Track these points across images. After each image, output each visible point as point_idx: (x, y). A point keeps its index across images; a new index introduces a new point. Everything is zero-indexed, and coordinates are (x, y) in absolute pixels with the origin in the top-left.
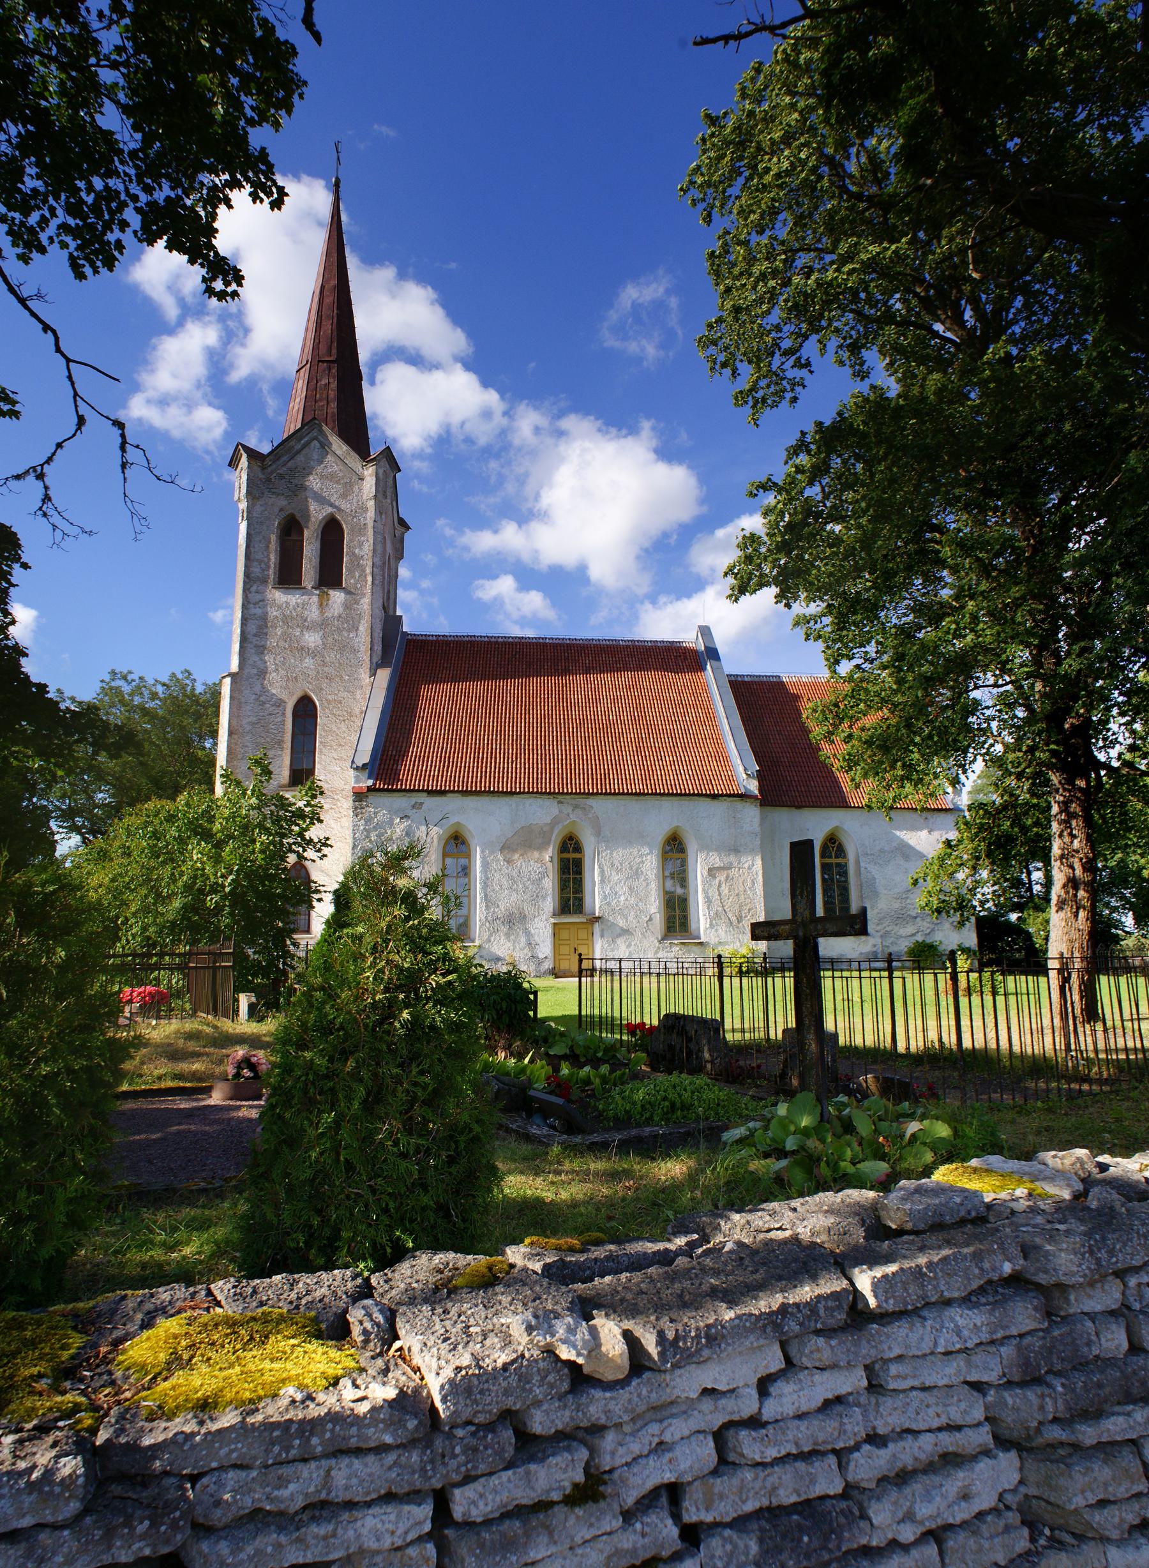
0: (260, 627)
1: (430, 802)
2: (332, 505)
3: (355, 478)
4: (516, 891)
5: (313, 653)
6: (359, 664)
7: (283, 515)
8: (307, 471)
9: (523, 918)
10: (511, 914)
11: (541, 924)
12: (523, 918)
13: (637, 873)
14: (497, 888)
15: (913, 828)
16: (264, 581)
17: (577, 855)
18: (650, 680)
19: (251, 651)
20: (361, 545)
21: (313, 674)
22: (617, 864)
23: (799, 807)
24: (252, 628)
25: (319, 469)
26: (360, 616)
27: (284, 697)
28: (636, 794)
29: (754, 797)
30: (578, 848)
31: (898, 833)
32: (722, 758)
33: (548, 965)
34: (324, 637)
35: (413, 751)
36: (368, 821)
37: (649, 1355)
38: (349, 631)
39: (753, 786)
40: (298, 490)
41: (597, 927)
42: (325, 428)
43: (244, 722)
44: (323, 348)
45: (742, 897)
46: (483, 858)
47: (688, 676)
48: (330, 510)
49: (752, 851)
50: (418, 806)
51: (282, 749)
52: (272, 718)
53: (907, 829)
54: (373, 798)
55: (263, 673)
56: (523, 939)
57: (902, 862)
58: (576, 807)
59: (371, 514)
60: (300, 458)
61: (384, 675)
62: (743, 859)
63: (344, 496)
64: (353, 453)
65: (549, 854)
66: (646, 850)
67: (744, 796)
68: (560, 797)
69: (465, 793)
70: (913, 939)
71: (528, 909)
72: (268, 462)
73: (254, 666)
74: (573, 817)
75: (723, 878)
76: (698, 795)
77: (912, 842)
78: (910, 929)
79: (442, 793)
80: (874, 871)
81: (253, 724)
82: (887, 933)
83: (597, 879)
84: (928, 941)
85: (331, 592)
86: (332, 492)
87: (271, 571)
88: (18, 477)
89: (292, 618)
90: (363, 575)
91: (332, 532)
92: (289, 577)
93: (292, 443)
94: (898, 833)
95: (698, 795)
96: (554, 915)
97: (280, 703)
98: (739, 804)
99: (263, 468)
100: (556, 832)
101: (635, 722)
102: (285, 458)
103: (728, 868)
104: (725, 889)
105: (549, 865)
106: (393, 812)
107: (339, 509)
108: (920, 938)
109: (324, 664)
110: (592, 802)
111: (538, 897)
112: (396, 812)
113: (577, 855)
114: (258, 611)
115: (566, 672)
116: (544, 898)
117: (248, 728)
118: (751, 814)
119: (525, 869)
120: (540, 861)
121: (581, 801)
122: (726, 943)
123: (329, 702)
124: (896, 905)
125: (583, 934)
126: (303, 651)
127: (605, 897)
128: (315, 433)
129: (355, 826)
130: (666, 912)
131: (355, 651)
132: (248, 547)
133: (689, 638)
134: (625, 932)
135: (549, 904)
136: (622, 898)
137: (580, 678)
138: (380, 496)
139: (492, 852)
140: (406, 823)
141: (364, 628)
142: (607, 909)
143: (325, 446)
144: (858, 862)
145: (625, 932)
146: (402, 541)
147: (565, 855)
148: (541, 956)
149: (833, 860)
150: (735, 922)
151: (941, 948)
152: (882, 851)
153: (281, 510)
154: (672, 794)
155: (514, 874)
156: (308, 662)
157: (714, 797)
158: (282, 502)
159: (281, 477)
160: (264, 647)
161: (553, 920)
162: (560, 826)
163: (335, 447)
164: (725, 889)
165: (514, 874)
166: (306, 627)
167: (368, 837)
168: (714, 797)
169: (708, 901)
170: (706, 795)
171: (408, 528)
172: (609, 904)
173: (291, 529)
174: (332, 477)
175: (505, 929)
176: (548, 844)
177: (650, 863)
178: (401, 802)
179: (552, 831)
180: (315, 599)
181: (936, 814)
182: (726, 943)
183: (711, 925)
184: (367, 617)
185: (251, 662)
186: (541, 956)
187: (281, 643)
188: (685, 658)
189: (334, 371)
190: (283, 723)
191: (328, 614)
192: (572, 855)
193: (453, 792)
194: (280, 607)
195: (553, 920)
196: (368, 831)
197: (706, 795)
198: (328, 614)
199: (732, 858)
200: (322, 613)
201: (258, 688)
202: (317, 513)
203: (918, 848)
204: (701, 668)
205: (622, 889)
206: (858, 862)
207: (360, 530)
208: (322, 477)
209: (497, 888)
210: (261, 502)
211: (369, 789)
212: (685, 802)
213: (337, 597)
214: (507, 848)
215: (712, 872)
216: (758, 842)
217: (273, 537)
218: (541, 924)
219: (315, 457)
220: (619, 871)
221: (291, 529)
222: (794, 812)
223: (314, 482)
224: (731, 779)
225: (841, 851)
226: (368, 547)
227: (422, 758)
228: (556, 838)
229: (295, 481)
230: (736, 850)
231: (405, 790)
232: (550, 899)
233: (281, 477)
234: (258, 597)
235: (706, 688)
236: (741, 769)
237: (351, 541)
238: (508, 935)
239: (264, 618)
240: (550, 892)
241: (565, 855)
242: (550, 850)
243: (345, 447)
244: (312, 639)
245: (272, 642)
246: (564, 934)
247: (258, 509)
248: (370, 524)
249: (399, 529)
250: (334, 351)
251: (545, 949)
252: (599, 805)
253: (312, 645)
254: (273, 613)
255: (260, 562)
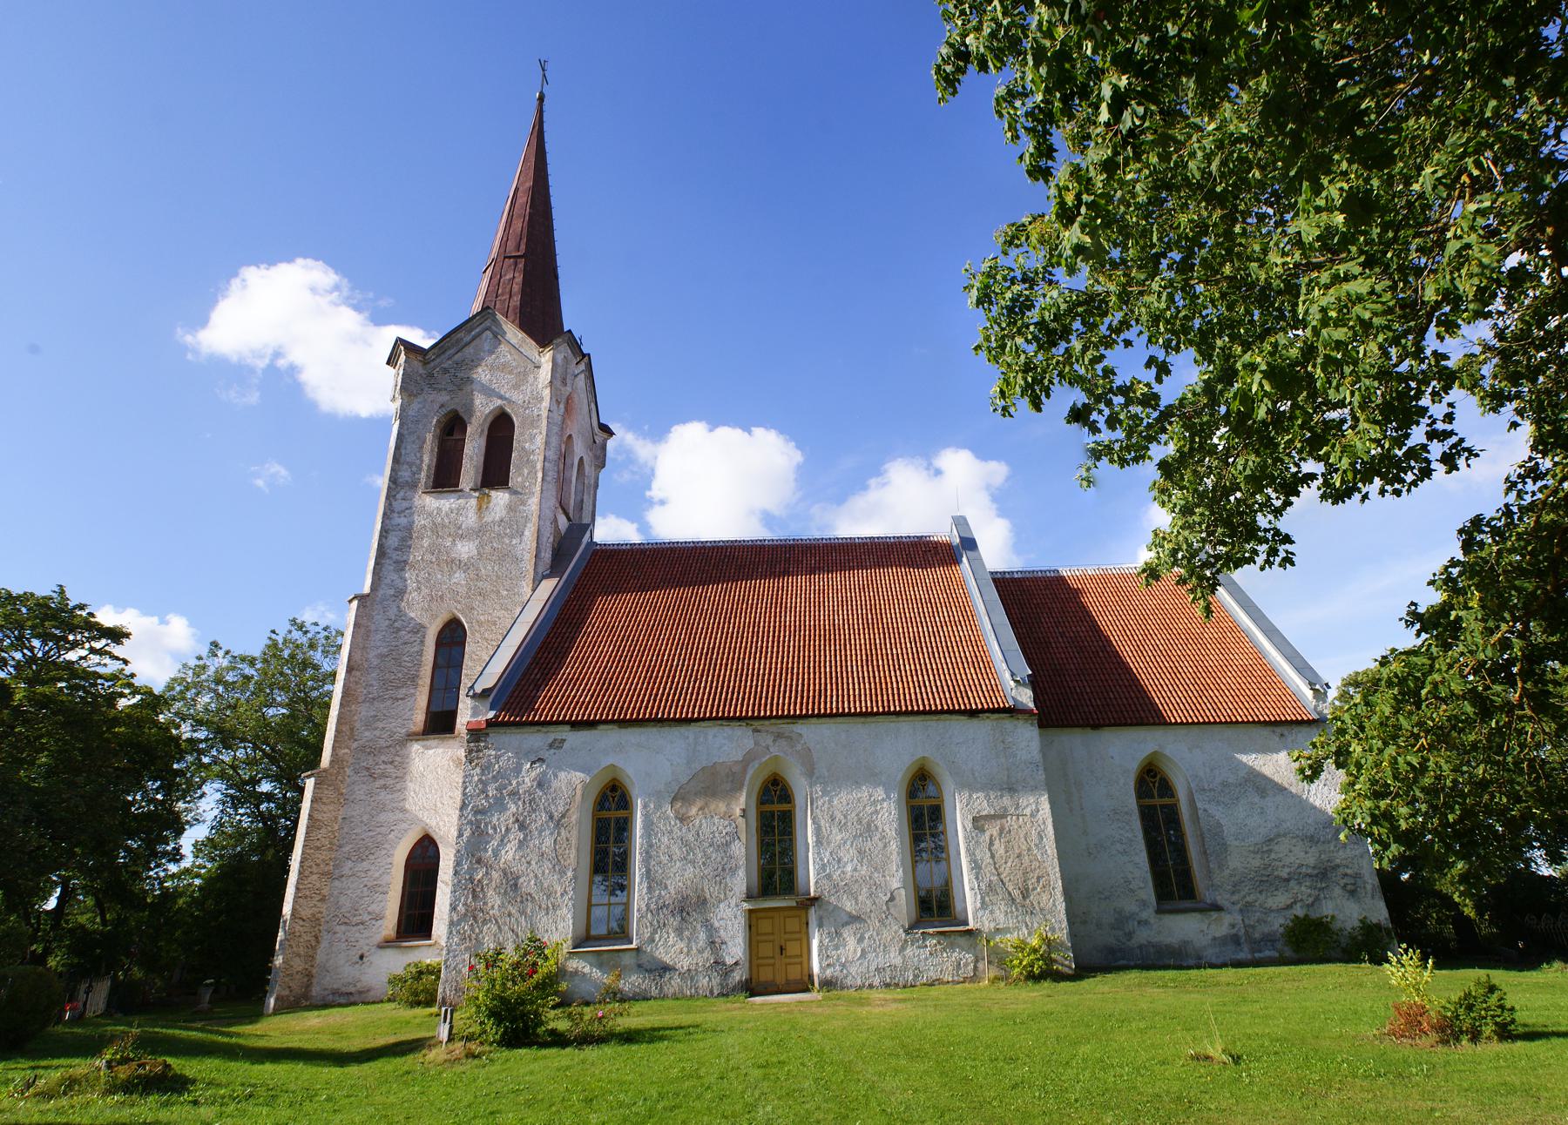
0: (403, 539)
1: (574, 738)
2: (501, 397)
3: (530, 366)
4: (693, 862)
5: (465, 566)
6: (522, 576)
7: (443, 411)
8: (475, 362)
9: (702, 903)
10: (685, 898)
11: (729, 913)
12: (702, 903)
13: (869, 829)
14: (665, 859)
15: (1266, 749)
16: (413, 486)
17: (785, 807)
18: (890, 578)
19: (389, 566)
20: (532, 438)
21: (463, 590)
22: (839, 816)
23: (1096, 726)
24: (393, 541)
25: (490, 359)
26: (527, 519)
27: (425, 621)
28: (861, 714)
29: (1028, 712)
30: (786, 796)
31: (1244, 758)
32: (982, 663)
33: (738, 976)
34: (481, 546)
35: (566, 672)
36: (485, 769)
37: (1244, 752)
38: (512, 537)
39: (1026, 697)
40: (463, 383)
41: (813, 914)
42: (499, 317)
43: (372, 654)
44: (511, 245)
45: (1026, 860)
46: (646, 816)
47: (940, 571)
48: (499, 402)
49: (1034, 789)
50: (556, 745)
51: (416, 686)
52: (407, 648)
53: (1257, 751)
54: (496, 737)
55: (400, 593)
56: (702, 936)
57: (1257, 799)
58: (779, 736)
59: (546, 404)
60: (469, 350)
61: (548, 586)
62: (1023, 802)
63: (516, 387)
64: (529, 340)
65: (741, 801)
66: (880, 793)
67: (1013, 711)
68: (756, 724)
69: (623, 723)
70: (1290, 914)
71: (710, 890)
72: (431, 356)
73: (391, 586)
74: (774, 750)
75: (995, 832)
76: (949, 712)
77: (1268, 770)
78: (1281, 899)
79: (591, 724)
80: (1218, 813)
81: (381, 656)
82: (1249, 905)
83: (811, 839)
84: (1314, 915)
85: (493, 493)
86: (503, 384)
87: (423, 475)
88: (541, 99)
89: (444, 526)
90: (533, 472)
91: (501, 429)
92: (445, 478)
93: (461, 335)
94: (1237, 756)
95: (949, 712)
96: (749, 897)
97: (419, 629)
98: (1008, 723)
99: (425, 363)
100: (750, 772)
101: (868, 625)
102: (452, 351)
103: (1002, 815)
104: (999, 848)
105: (741, 822)
106: (521, 754)
107: (509, 401)
108: (1299, 911)
109: (478, 577)
110: (800, 728)
111: (725, 870)
112: (526, 754)
113: (785, 807)
114: (403, 521)
115: (785, 573)
116: (733, 871)
117: (375, 662)
118: (1027, 737)
119: (706, 830)
120: (728, 816)
121: (785, 727)
122: (1007, 930)
123: (480, 624)
124: (1256, 862)
125: (792, 924)
126: (455, 564)
127: (823, 867)
128: (488, 323)
129: (467, 777)
130: (907, 802)
131: (517, 560)
132: (397, 448)
133: (943, 532)
134: (855, 919)
135: (740, 882)
136: (849, 868)
137: (801, 580)
138: (558, 383)
139: (658, 807)
140: (539, 769)
141: (530, 533)
142: (826, 884)
143: (498, 336)
144: (1192, 803)
145: (855, 919)
146: (604, 447)
147: (768, 808)
148: (729, 961)
149: (1157, 801)
150: (1019, 899)
151: (1336, 926)
152: (1225, 784)
153: (442, 406)
154: (912, 713)
155: (690, 837)
156: (459, 577)
157: (973, 713)
158: (444, 397)
159: (446, 371)
160: (405, 562)
161: (746, 906)
162: (756, 764)
163: (509, 336)
164: (999, 848)
165: (690, 837)
166: (460, 535)
167: (483, 791)
168: (973, 713)
169: (976, 867)
170: (960, 712)
171: (611, 433)
172: (829, 877)
173: (453, 427)
174: (504, 367)
175: (674, 922)
176: (740, 788)
177: (889, 815)
178: (535, 740)
179: (744, 771)
180: (473, 502)
181: (1296, 729)
182: (1007, 930)
183: (984, 905)
184: (535, 519)
185: (388, 581)
186: (729, 961)
187: (428, 557)
188: (937, 553)
189: (521, 266)
190: (420, 652)
191: (488, 519)
192: (778, 807)
193: (606, 722)
194: (430, 514)
195: (746, 906)
196: (485, 784)
197: (960, 712)
198: (488, 519)
199: (1007, 801)
200: (480, 518)
201: (392, 613)
202: (482, 408)
203: (1276, 779)
204: (956, 561)
205: (848, 854)
206: (1192, 803)
207: (533, 422)
208: (492, 368)
209: (665, 859)
210: (420, 399)
211: (489, 723)
212: (933, 723)
213: (500, 498)
214: (680, 796)
215: (978, 822)
216: (1041, 776)
217: (429, 437)
218: (729, 913)
219: (487, 348)
220: (842, 827)
221: (453, 427)
222: (1090, 734)
223: (482, 374)
224: (995, 689)
225: (1166, 788)
226: (540, 440)
227: (573, 682)
228: (754, 778)
229: (461, 375)
230: (1011, 789)
231: (539, 723)
232: (741, 873)
233: (446, 371)
234: (405, 504)
235: (962, 585)
236: (1007, 675)
237: (522, 434)
238: (679, 932)
239: (409, 528)
240: (742, 862)
241: (768, 808)
242: (743, 799)
243: (521, 335)
244: (465, 549)
245: (415, 556)
246: (765, 926)
247: (415, 406)
248: (544, 414)
249: (600, 435)
250: (523, 247)
251: (736, 950)
252: (810, 732)
253: (465, 557)
254: (420, 521)
255: (410, 465)
